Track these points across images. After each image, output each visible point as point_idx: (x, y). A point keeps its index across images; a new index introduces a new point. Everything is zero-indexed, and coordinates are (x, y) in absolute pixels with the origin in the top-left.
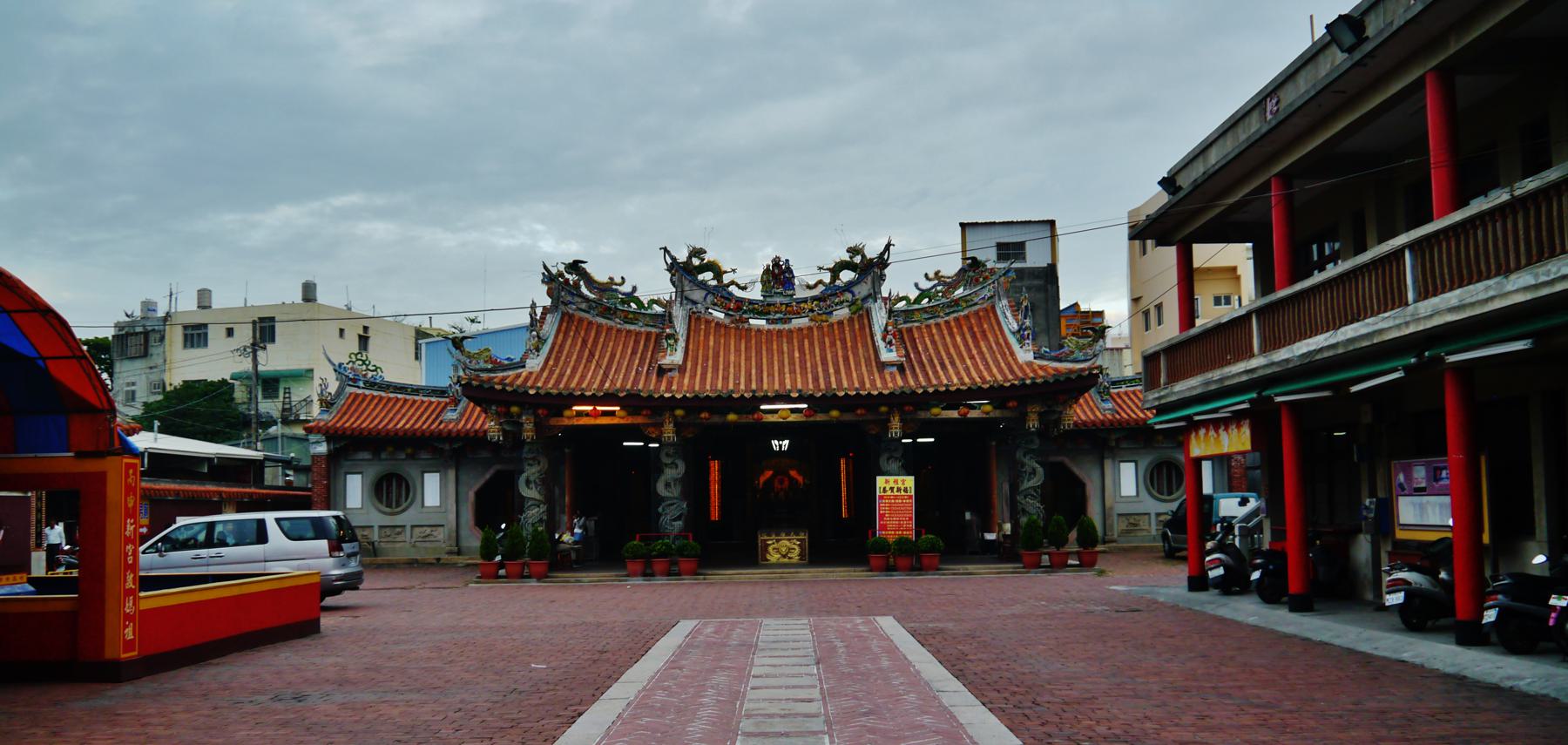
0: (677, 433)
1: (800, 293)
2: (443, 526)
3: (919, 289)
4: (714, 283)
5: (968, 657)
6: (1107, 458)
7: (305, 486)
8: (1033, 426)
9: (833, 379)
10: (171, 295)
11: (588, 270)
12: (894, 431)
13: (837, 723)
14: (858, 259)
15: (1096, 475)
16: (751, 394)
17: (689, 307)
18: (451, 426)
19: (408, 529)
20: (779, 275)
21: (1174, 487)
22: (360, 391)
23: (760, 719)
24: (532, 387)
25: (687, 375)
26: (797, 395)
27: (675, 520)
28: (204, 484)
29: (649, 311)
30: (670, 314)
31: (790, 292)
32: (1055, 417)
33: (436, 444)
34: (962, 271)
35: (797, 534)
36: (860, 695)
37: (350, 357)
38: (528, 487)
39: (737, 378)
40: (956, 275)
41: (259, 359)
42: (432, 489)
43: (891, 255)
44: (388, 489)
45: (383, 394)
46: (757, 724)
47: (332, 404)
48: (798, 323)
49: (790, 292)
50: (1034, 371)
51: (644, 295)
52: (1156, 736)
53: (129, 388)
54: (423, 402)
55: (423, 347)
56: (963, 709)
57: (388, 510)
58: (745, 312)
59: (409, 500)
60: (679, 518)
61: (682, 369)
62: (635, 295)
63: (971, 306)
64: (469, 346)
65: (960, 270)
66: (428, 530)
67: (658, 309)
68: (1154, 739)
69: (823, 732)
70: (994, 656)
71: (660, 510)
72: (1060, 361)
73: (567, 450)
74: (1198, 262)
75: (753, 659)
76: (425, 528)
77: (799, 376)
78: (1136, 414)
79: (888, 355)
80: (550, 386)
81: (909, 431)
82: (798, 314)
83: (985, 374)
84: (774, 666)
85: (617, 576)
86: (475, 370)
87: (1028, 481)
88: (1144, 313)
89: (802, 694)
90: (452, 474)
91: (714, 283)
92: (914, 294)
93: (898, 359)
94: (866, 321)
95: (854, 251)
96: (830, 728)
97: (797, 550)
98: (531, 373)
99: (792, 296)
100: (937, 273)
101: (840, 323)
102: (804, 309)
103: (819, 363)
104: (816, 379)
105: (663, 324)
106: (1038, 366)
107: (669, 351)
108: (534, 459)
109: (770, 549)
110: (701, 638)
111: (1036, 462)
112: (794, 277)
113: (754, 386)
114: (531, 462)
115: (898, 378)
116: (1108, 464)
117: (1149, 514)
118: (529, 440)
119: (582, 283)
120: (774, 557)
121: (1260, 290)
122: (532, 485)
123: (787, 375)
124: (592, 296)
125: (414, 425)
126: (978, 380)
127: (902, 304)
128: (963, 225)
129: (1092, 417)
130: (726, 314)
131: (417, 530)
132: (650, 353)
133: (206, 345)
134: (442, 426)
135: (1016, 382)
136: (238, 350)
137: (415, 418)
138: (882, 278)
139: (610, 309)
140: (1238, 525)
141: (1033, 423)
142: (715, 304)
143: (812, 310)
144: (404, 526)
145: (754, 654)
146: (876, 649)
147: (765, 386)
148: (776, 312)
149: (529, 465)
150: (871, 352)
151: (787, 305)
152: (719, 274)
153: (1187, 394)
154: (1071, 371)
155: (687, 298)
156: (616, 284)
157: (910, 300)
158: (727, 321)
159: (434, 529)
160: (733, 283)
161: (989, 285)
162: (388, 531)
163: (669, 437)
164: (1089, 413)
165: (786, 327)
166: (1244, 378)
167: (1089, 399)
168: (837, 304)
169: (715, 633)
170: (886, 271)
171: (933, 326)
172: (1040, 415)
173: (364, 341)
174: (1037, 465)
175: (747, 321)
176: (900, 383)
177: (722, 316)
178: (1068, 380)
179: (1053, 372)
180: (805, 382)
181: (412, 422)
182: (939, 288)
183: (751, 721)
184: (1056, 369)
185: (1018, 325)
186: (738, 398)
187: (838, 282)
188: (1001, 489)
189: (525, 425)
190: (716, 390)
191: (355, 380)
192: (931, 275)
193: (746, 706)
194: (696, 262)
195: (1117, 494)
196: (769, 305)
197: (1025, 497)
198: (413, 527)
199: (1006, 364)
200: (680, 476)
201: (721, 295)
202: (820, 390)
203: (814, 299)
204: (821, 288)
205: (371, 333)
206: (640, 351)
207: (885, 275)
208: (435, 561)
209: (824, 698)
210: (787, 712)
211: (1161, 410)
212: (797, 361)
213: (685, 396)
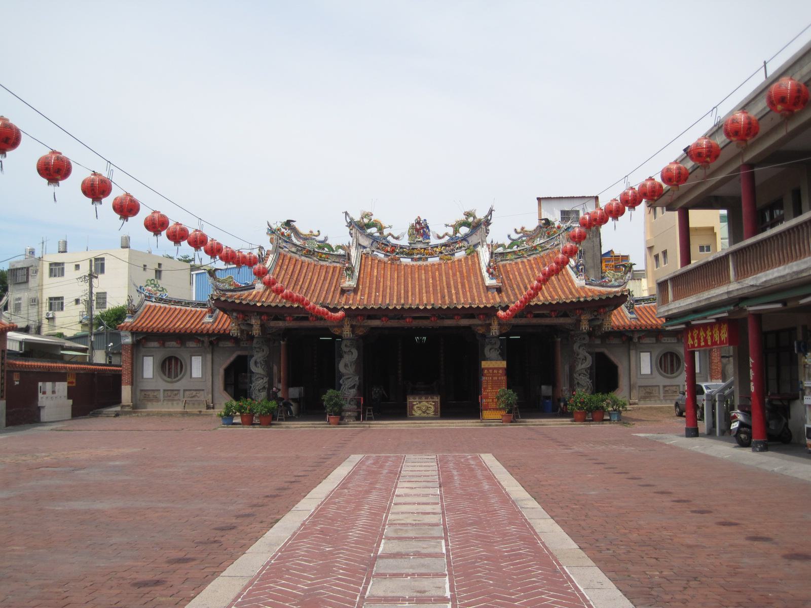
0: (353, 332)
1: (433, 241)
2: (203, 390)
3: (510, 239)
4: (378, 234)
5: (542, 483)
6: (632, 350)
7: (119, 364)
8: (585, 329)
9: (454, 297)
10: (43, 243)
11: (297, 227)
12: (494, 331)
13: (451, 530)
14: (471, 219)
15: (625, 363)
16: (401, 307)
17: (361, 250)
18: (208, 326)
19: (182, 392)
20: (420, 229)
21: (675, 369)
22: (153, 304)
23: (399, 527)
24: (258, 302)
25: (359, 294)
26: (431, 307)
27: (350, 388)
28: (28, 361)
29: (336, 253)
30: (348, 254)
31: (427, 241)
32: (599, 323)
33: (199, 338)
34: (540, 227)
35: (432, 398)
36: (468, 510)
37: (147, 282)
38: (256, 366)
39: (391, 296)
40: (535, 230)
41: (93, 284)
42: (197, 367)
43: (492, 217)
44: (169, 366)
45: (167, 306)
46: (396, 531)
47: (136, 312)
48: (431, 260)
49: (427, 241)
50: (586, 292)
51: (333, 243)
52: (670, 541)
53: (17, 302)
54: (191, 311)
55: (194, 276)
56: (538, 521)
57: (169, 380)
58: (397, 254)
59: (183, 373)
60: (353, 387)
61: (355, 290)
62: (327, 242)
63: (545, 250)
64: (218, 274)
65: (538, 227)
66: (194, 393)
67: (341, 252)
68: (669, 544)
69: (441, 538)
70: (559, 483)
71: (341, 382)
72: (603, 286)
73: (282, 342)
74: (692, 224)
75: (397, 483)
76: (192, 391)
77: (432, 295)
78: (651, 321)
79: (489, 282)
80: (270, 300)
81: (504, 332)
82: (431, 255)
83: (553, 293)
84: (412, 488)
85: (313, 424)
86: (223, 290)
87: (582, 364)
88: (657, 256)
89: (428, 508)
90: (209, 357)
91: (378, 234)
92: (507, 242)
93: (497, 284)
94: (476, 259)
95: (468, 214)
96: (446, 534)
97: (433, 409)
98: (258, 292)
99: (428, 243)
100: (523, 229)
101: (460, 261)
102: (436, 251)
103: (445, 286)
104: (443, 297)
105: (345, 261)
106: (589, 289)
107: (348, 279)
108: (260, 348)
109: (415, 407)
110: (364, 467)
111: (587, 352)
112: (429, 231)
113: (402, 301)
114: (258, 350)
115: (497, 296)
116: (633, 353)
117: (659, 386)
118: (256, 336)
119: (292, 234)
120: (417, 413)
121: (732, 240)
122: (259, 365)
123: (424, 295)
124: (298, 243)
125: (185, 325)
126: (549, 298)
127: (500, 250)
128: (539, 199)
129: (623, 323)
130: (386, 255)
131: (187, 393)
132: (335, 280)
133: (63, 275)
134: (203, 327)
135: (574, 300)
136: (80, 278)
137: (186, 321)
138: (487, 232)
139: (310, 251)
140: (718, 394)
141: (585, 327)
142: (378, 249)
143: (441, 253)
144: (179, 390)
145: (398, 479)
146: (481, 477)
147: (410, 302)
148: (418, 254)
149: (257, 352)
150: (480, 280)
151: (425, 249)
152: (381, 229)
153: (687, 308)
154: (610, 293)
155: (359, 245)
156: (314, 236)
157: (505, 246)
158: (386, 259)
159: (198, 392)
160: (390, 234)
161: (557, 236)
162: (169, 393)
163: (347, 334)
164: (620, 320)
165: (425, 263)
166: (725, 297)
167: (621, 312)
168: (457, 249)
169: (374, 464)
170: (490, 227)
171: (520, 264)
172: (590, 321)
173: (158, 273)
174: (587, 354)
175: (399, 259)
176: (498, 300)
177: (382, 256)
178: (608, 298)
179: (598, 294)
180: (436, 299)
181: (184, 324)
182: (524, 238)
183: (393, 528)
184: (600, 292)
185: (575, 262)
186: (392, 309)
187: (458, 235)
188: (563, 370)
189: (254, 326)
190: (378, 304)
191: (150, 297)
192: (519, 230)
193: (390, 517)
194: (366, 221)
195: (639, 373)
196: (413, 249)
197: (580, 375)
198: (185, 390)
199: (567, 288)
200: (354, 360)
201: (380, 242)
202: (446, 304)
203: (445, 245)
204: (447, 238)
205: (163, 268)
206: (329, 278)
207: (489, 230)
208: (198, 413)
209: (443, 513)
210: (417, 522)
211: (669, 318)
212: (431, 285)
213: (357, 308)
